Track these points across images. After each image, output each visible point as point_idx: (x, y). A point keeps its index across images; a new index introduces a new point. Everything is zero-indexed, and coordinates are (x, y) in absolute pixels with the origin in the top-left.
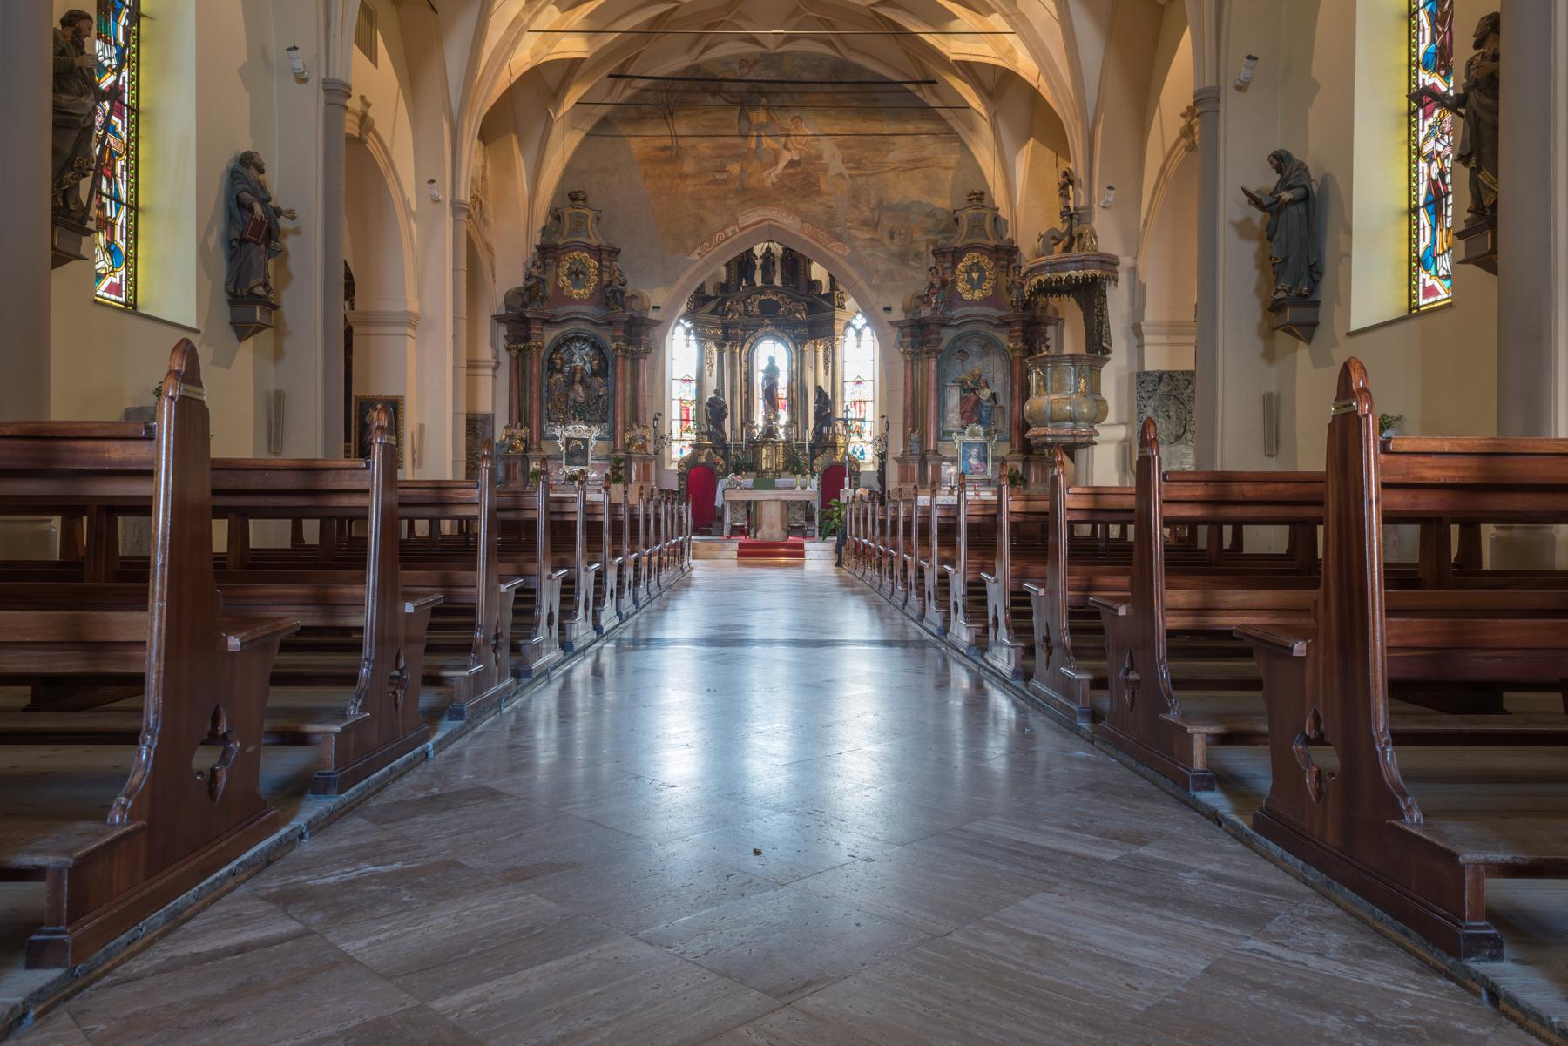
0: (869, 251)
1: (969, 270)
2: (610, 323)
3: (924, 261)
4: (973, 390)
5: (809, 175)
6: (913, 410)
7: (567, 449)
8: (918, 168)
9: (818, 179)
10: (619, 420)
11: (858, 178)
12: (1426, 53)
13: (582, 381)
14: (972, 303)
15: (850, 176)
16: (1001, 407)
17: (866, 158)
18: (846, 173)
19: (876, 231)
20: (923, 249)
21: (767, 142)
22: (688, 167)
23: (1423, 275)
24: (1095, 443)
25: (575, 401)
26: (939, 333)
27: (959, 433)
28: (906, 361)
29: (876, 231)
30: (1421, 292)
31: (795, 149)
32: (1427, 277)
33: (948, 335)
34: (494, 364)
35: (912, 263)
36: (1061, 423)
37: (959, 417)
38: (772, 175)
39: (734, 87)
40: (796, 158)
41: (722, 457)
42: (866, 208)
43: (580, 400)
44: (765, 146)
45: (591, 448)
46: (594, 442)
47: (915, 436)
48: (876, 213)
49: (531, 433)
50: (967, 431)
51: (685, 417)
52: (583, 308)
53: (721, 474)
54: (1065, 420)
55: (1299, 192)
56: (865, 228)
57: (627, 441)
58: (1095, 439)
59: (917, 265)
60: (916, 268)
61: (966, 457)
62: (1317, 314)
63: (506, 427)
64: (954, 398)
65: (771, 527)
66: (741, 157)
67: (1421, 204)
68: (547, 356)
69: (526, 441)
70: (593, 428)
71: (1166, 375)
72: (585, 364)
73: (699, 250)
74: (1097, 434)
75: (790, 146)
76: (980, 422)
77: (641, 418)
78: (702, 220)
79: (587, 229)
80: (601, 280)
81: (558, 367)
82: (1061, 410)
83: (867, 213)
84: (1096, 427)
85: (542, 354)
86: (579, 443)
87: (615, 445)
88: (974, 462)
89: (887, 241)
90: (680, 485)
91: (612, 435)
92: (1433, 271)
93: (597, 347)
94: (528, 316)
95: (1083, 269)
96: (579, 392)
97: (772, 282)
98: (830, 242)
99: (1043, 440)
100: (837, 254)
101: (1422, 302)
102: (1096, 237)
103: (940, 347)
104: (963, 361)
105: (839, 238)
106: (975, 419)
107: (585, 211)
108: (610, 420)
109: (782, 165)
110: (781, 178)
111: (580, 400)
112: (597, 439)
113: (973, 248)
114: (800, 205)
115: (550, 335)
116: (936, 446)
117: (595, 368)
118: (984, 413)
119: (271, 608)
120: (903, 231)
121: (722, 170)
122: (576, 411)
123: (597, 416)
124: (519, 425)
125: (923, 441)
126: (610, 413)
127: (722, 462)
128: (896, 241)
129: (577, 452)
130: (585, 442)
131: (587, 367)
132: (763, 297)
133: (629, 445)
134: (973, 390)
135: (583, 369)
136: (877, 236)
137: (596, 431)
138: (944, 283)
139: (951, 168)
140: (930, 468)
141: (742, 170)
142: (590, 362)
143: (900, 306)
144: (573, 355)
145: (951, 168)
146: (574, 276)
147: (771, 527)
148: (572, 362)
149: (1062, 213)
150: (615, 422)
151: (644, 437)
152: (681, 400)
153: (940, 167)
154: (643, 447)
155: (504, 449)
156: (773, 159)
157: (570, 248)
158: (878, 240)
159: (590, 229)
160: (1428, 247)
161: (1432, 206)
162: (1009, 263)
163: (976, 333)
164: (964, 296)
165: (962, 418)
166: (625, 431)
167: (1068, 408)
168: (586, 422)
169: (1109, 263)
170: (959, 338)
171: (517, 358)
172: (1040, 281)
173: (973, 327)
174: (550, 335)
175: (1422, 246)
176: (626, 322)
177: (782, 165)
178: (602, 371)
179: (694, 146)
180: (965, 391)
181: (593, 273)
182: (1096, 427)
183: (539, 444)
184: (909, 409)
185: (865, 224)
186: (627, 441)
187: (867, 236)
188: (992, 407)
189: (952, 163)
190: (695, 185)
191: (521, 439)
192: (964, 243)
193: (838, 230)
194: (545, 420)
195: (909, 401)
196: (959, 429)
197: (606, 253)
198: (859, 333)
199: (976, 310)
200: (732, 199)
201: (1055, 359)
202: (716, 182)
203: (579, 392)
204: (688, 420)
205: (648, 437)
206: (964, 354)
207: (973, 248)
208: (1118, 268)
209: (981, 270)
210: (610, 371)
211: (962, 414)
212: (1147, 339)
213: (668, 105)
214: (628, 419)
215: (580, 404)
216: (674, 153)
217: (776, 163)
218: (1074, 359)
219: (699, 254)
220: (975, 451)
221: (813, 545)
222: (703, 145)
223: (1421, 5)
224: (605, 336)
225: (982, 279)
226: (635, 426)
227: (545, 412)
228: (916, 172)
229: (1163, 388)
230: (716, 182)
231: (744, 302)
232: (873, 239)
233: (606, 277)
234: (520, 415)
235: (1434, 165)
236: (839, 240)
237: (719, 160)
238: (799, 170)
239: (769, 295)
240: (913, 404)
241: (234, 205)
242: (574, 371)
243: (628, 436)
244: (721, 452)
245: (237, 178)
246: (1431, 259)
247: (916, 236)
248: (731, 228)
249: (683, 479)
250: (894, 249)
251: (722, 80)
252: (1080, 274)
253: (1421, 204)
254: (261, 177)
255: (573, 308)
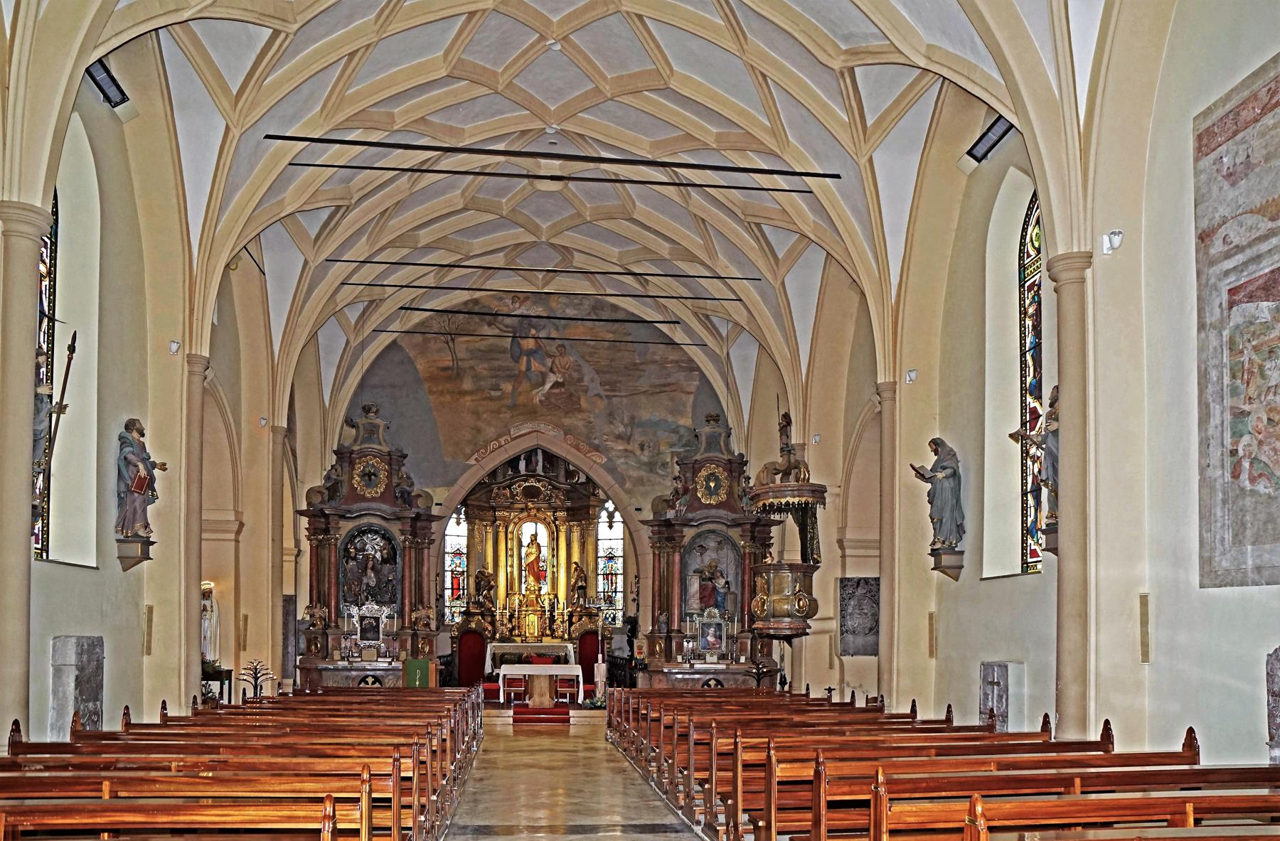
0: (622, 460)
1: (708, 479)
2: (399, 519)
3: (669, 470)
4: (710, 579)
5: (571, 395)
6: (660, 595)
7: (361, 625)
8: (664, 392)
9: (579, 399)
10: (407, 602)
11: (614, 399)
12: (1031, 384)
13: (373, 569)
14: (709, 506)
15: (607, 396)
16: (733, 593)
17: (620, 382)
18: (603, 393)
19: (629, 444)
20: (668, 460)
21: (535, 365)
22: (467, 385)
23: (1030, 541)
24: (808, 634)
25: (368, 585)
26: (682, 532)
27: (699, 615)
28: (654, 554)
29: (629, 444)
30: (1028, 552)
31: (560, 372)
32: (1032, 543)
33: (689, 533)
34: (296, 552)
35: (660, 472)
36: (781, 619)
37: (698, 601)
38: (538, 395)
39: (508, 321)
40: (560, 380)
41: (489, 623)
42: (620, 425)
43: (373, 584)
44: (533, 369)
45: (382, 626)
46: (385, 620)
47: (663, 618)
48: (629, 430)
49: (330, 612)
50: (705, 614)
51: (455, 586)
52: (374, 505)
53: (489, 638)
54: (784, 616)
55: (949, 471)
56: (620, 441)
57: (413, 620)
58: (808, 631)
59: (663, 473)
60: (663, 476)
61: (704, 635)
62: (962, 560)
63: (308, 607)
64: (694, 586)
65: (541, 698)
66: (515, 378)
67: (1029, 490)
68: (343, 547)
69: (325, 620)
70: (384, 608)
71: (862, 581)
72: (376, 552)
73: (476, 456)
74: (810, 627)
75: (555, 369)
76: (717, 606)
77: (425, 600)
78: (479, 430)
79: (378, 437)
80: (390, 482)
81: (353, 555)
82: (781, 608)
83: (621, 429)
84: (809, 621)
85: (339, 545)
86: (372, 621)
87: (403, 622)
88: (711, 639)
89: (638, 452)
90: (452, 647)
91: (401, 614)
92: (1035, 539)
93: (387, 538)
94: (327, 512)
95: (799, 496)
96: (371, 579)
97: (535, 470)
98: (589, 452)
99: (767, 631)
100: (595, 462)
101: (1029, 560)
102: (808, 472)
103: (683, 543)
104: (701, 554)
105: (597, 448)
106: (712, 603)
107: (378, 421)
108: (399, 601)
109: (548, 386)
110: (548, 396)
111: (373, 584)
112: (387, 617)
113: (710, 461)
114: (563, 420)
115: (346, 527)
116: (680, 626)
117: (385, 556)
118: (719, 599)
119: (247, 808)
120: (651, 444)
121: (497, 388)
122: (369, 593)
123: (387, 597)
124: (318, 605)
125: (669, 622)
126: (399, 596)
127: (490, 628)
128: (646, 452)
129: (370, 629)
130: (377, 619)
131: (378, 555)
132: (527, 484)
133: (415, 623)
134: (710, 579)
135: (374, 557)
136: (629, 448)
137: (386, 611)
138: (686, 491)
139: (692, 393)
140: (674, 644)
141: (514, 389)
142: (381, 551)
143: (649, 506)
144: (366, 544)
145: (692, 393)
146: (367, 478)
147: (541, 698)
148: (364, 550)
149: (781, 449)
150: (403, 604)
151: (429, 617)
152: (452, 571)
153: (682, 392)
154: (427, 625)
155: (306, 626)
156: (541, 380)
157: (362, 454)
158: (630, 452)
159: (381, 437)
160: (1033, 522)
161: (1035, 493)
162: (740, 475)
163: (713, 532)
164: (703, 500)
165: (701, 602)
166: (412, 611)
167: (786, 607)
168: (377, 603)
169: (819, 492)
170: (699, 535)
171: (317, 547)
172: (764, 504)
173: (711, 526)
174: (346, 527)
175: (1030, 520)
176: (412, 518)
177: (548, 386)
178: (390, 559)
179: (472, 368)
180: (703, 580)
181: (382, 475)
182: (809, 621)
183: (336, 622)
184: (657, 594)
185: (619, 437)
186: (413, 620)
187: (621, 448)
188: (725, 594)
189: (692, 389)
190: (473, 401)
191: (321, 617)
192: (703, 456)
193: (596, 442)
194: (342, 601)
195: (657, 588)
196: (699, 612)
197: (395, 459)
198: (611, 516)
199: (713, 512)
200: (505, 413)
201: (777, 567)
202: (491, 399)
203: (371, 579)
204: (459, 589)
205: (431, 616)
206: (703, 549)
207: (710, 461)
208: (826, 495)
209: (717, 480)
210: (398, 560)
211: (701, 599)
212: (848, 552)
213: (451, 334)
214: (413, 601)
215: (372, 588)
216: (455, 372)
217: (543, 384)
218: (792, 567)
219: (476, 459)
220: (712, 630)
221: (506, 345)
222: (480, 367)
223: (1027, 349)
224: (395, 528)
225: (718, 487)
226: (420, 607)
227: (341, 594)
228: (662, 394)
229: (860, 591)
230: (491, 399)
231: (510, 489)
232: (626, 450)
233: (395, 480)
234: (318, 597)
235: (1036, 465)
236: (598, 451)
237: (494, 380)
238: (563, 390)
239: (532, 482)
240: (660, 589)
241: (122, 464)
242: (367, 557)
243: (414, 615)
244: (489, 619)
245: (125, 442)
246: (1034, 531)
247: (662, 448)
248: (504, 438)
249: (455, 643)
250: (645, 459)
251: (497, 315)
252: (796, 500)
253: (1029, 490)
254: (142, 439)
255: (365, 505)
